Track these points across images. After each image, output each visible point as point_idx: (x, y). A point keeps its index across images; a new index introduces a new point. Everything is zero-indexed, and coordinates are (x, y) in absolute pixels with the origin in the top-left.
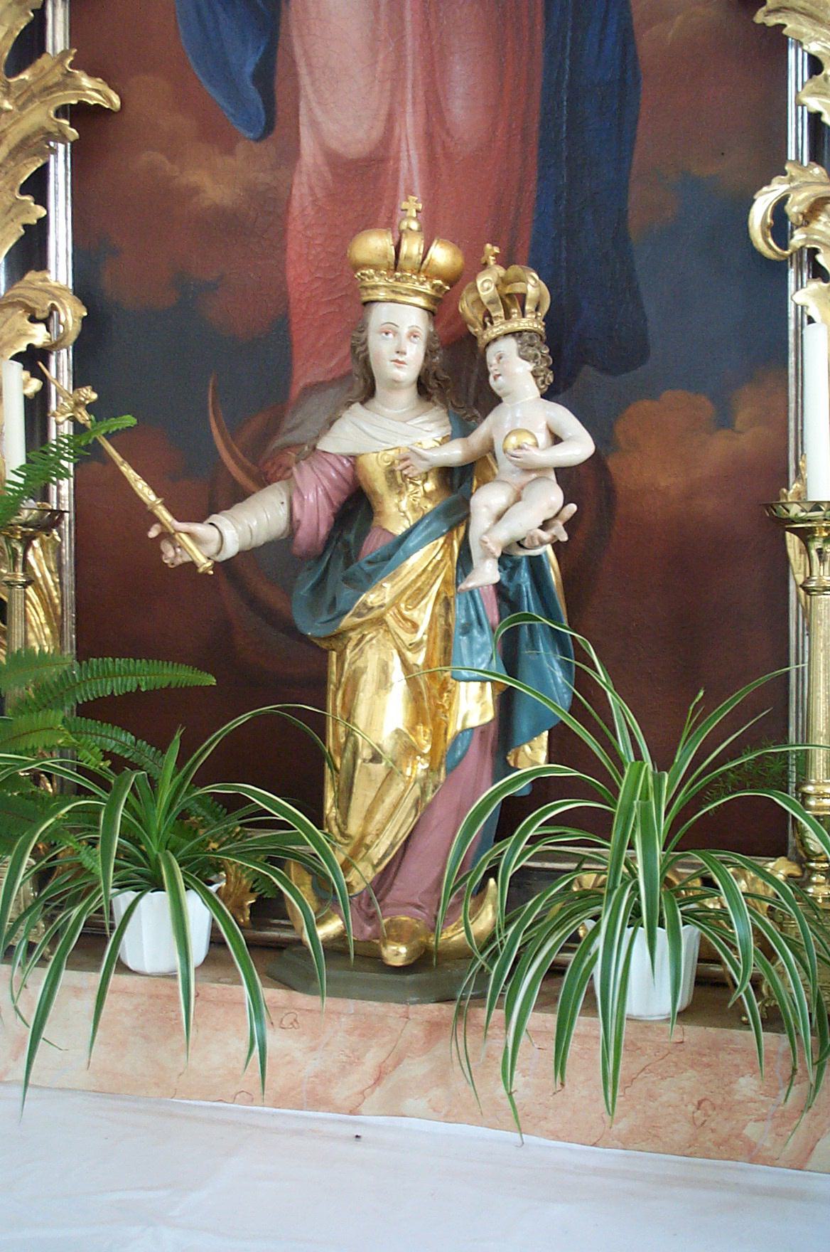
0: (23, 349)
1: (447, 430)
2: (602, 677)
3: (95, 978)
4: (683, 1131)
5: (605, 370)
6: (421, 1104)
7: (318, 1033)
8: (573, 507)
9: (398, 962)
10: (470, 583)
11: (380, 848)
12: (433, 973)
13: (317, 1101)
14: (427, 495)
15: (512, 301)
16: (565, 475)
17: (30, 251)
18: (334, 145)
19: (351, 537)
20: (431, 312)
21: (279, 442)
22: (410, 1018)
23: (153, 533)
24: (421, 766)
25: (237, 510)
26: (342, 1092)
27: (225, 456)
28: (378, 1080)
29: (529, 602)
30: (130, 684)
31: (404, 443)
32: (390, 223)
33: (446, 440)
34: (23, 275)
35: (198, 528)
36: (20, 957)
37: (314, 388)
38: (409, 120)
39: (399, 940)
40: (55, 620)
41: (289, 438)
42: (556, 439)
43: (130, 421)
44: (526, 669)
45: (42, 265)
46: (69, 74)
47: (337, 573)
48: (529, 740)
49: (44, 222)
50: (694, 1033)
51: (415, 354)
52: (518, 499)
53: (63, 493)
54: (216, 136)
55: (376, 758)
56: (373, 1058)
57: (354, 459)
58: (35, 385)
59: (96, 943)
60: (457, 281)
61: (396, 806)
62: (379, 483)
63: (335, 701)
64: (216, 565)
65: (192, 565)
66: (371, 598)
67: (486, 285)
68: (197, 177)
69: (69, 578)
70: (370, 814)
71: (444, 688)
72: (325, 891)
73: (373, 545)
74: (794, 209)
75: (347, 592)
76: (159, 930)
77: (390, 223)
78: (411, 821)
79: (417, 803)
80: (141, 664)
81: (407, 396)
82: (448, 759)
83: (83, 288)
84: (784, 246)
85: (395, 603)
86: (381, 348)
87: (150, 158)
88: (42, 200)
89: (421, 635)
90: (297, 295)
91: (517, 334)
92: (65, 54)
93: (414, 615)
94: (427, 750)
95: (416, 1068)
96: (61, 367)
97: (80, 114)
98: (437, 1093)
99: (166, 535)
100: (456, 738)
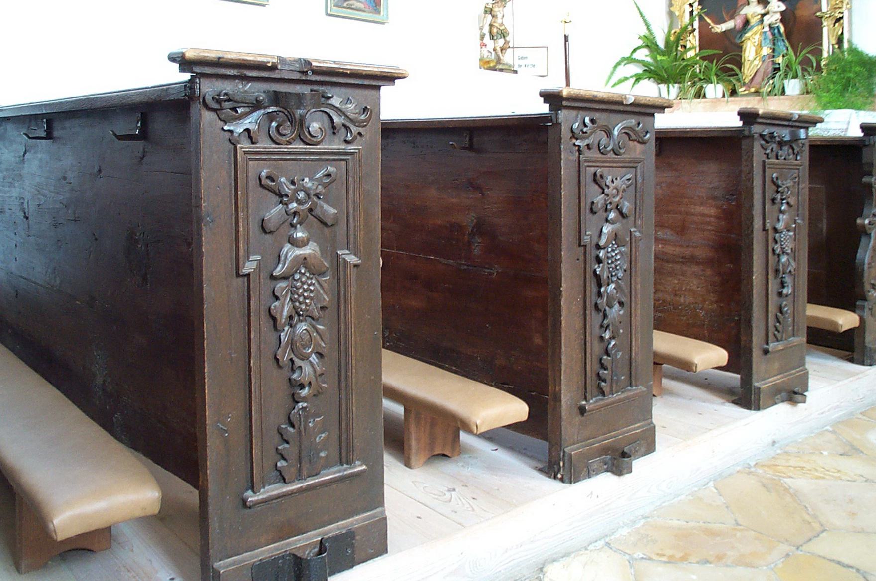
29: (777, 35)
53: (696, 25)
90: (336, 101)
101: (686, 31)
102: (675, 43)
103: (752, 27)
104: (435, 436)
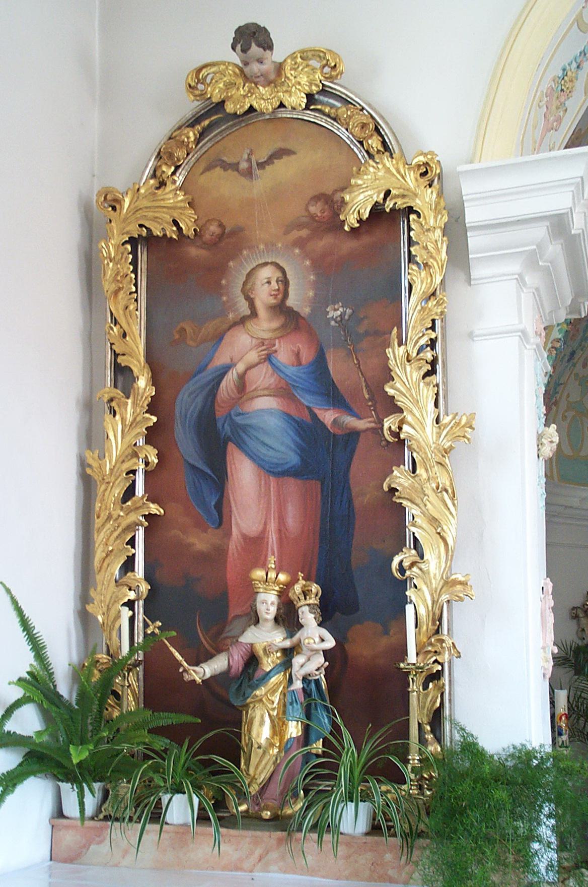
0: (126, 600)
1: (285, 635)
2: (339, 721)
3: (158, 827)
4: (367, 873)
5: (343, 613)
6: (276, 868)
7: (238, 844)
8: (327, 663)
9: (267, 817)
10: (292, 688)
11: (262, 777)
12: (279, 822)
13: (237, 868)
14: (278, 658)
15: (305, 593)
16: (326, 653)
17: (129, 565)
18: (244, 531)
19: (251, 671)
20: (279, 596)
21: (224, 635)
22: (271, 837)
23: (181, 670)
24: (276, 750)
25: (209, 662)
26: (247, 865)
27: (203, 639)
28: (260, 860)
30: (170, 722)
31: (269, 640)
32: (264, 565)
33: (285, 639)
34: (126, 574)
35: (197, 669)
36: (127, 820)
37: (237, 617)
38: (273, 524)
39: (267, 810)
40: (136, 699)
41: (228, 634)
42: (323, 640)
43: (174, 633)
44: (313, 717)
45: (133, 570)
46: (144, 504)
47: (245, 685)
48: (315, 742)
49: (134, 555)
50: (370, 839)
51: (273, 610)
52: (309, 660)
54: (200, 525)
55: (259, 747)
56: (258, 852)
57: (252, 645)
58: (131, 613)
59: (157, 816)
60: (289, 585)
61: (266, 764)
62: (261, 653)
63: (245, 728)
64: (203, 681)
65: (194, 681)
66: (258, 692)
67: (298, 588)
68: (192, 540)
69: (142, 683)
70: (257, 767)
71: (284, 723)
72: (242, 796)
73: (258, 675)
74: (406, 564)
75: (249, 690)
76: (179, 809)
77: (264, 565)
78: (272, 769)
79: (274, 763)
80: (173, 715)
81: (271, 624)
82: (286, 748)
83: (148, 578)
84: (403, 575)
85: (266, 694)
86: (261, 608)
87: (175, 532)
88: (133, 547)
89: (275, 705)
91: (309, 605)
92: (143, 496)
93: (273, 698)
94: (278, 745)
95: (274, 855)
96: (140, 607)
97: (149, 517)
98: (281, 864)
99: (185, 671)
100: (288, 740)
101: (117, 666)
102: (97, 687)
103: (268, 675)
104: (39, 733)
